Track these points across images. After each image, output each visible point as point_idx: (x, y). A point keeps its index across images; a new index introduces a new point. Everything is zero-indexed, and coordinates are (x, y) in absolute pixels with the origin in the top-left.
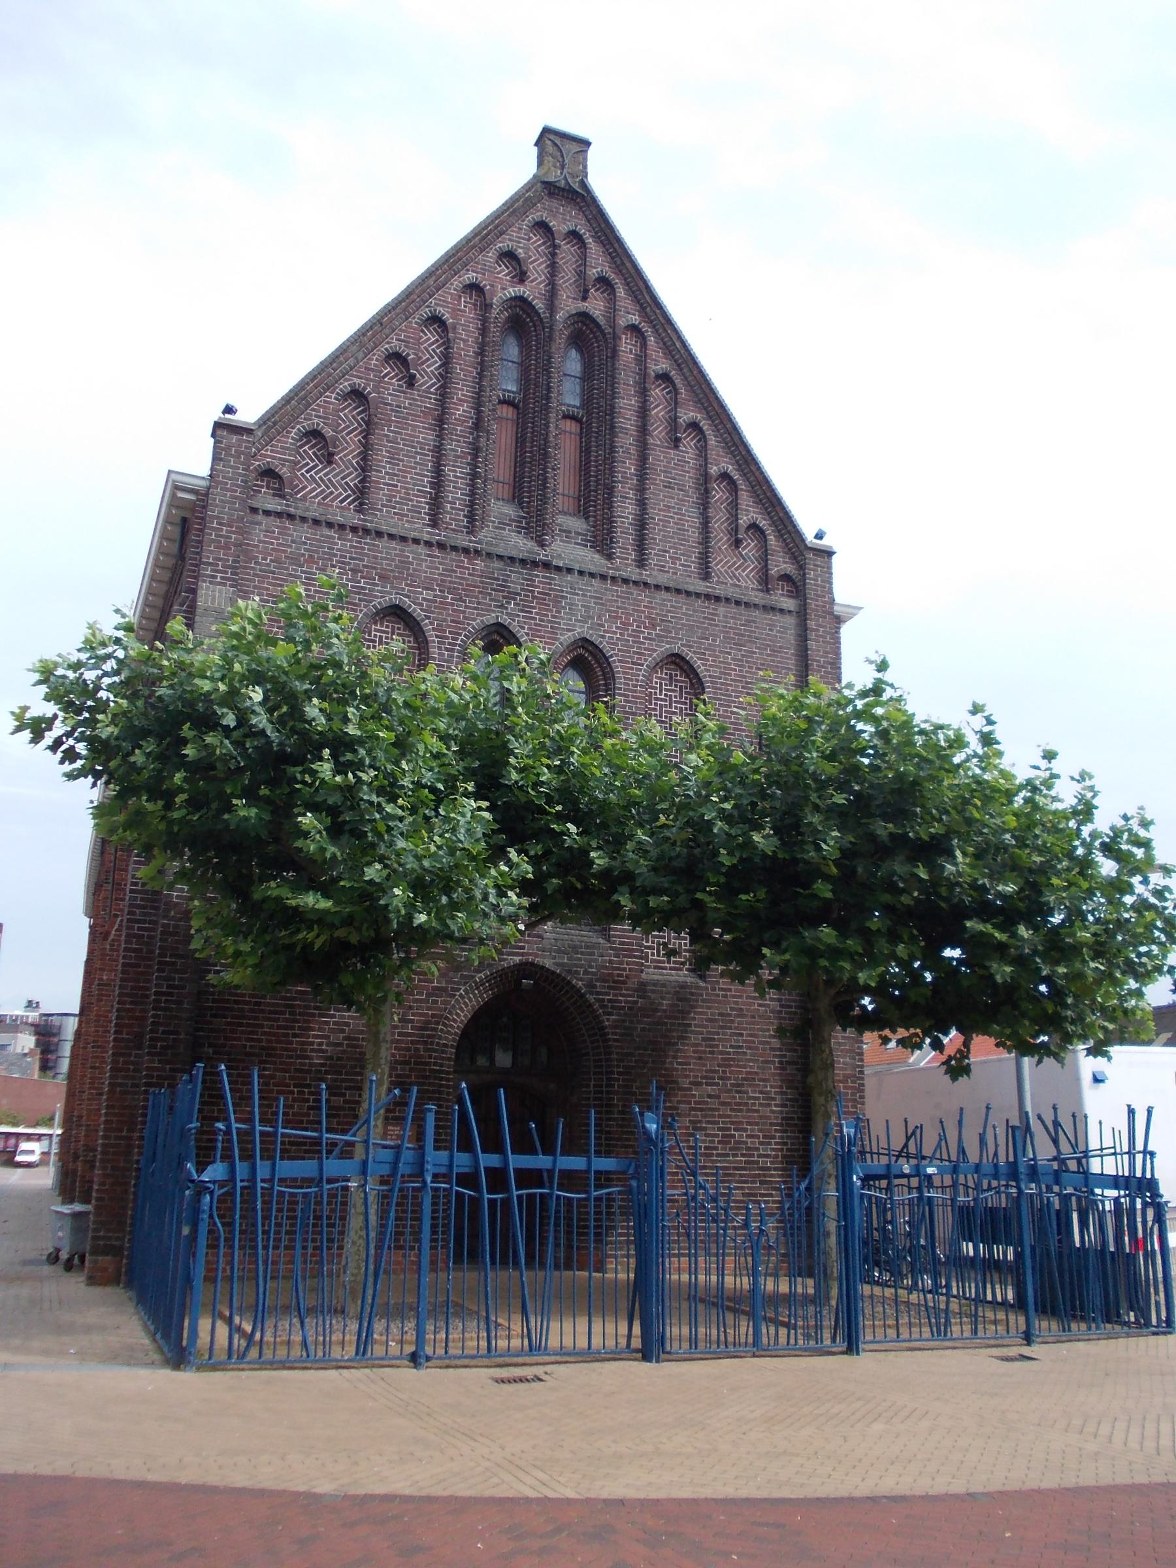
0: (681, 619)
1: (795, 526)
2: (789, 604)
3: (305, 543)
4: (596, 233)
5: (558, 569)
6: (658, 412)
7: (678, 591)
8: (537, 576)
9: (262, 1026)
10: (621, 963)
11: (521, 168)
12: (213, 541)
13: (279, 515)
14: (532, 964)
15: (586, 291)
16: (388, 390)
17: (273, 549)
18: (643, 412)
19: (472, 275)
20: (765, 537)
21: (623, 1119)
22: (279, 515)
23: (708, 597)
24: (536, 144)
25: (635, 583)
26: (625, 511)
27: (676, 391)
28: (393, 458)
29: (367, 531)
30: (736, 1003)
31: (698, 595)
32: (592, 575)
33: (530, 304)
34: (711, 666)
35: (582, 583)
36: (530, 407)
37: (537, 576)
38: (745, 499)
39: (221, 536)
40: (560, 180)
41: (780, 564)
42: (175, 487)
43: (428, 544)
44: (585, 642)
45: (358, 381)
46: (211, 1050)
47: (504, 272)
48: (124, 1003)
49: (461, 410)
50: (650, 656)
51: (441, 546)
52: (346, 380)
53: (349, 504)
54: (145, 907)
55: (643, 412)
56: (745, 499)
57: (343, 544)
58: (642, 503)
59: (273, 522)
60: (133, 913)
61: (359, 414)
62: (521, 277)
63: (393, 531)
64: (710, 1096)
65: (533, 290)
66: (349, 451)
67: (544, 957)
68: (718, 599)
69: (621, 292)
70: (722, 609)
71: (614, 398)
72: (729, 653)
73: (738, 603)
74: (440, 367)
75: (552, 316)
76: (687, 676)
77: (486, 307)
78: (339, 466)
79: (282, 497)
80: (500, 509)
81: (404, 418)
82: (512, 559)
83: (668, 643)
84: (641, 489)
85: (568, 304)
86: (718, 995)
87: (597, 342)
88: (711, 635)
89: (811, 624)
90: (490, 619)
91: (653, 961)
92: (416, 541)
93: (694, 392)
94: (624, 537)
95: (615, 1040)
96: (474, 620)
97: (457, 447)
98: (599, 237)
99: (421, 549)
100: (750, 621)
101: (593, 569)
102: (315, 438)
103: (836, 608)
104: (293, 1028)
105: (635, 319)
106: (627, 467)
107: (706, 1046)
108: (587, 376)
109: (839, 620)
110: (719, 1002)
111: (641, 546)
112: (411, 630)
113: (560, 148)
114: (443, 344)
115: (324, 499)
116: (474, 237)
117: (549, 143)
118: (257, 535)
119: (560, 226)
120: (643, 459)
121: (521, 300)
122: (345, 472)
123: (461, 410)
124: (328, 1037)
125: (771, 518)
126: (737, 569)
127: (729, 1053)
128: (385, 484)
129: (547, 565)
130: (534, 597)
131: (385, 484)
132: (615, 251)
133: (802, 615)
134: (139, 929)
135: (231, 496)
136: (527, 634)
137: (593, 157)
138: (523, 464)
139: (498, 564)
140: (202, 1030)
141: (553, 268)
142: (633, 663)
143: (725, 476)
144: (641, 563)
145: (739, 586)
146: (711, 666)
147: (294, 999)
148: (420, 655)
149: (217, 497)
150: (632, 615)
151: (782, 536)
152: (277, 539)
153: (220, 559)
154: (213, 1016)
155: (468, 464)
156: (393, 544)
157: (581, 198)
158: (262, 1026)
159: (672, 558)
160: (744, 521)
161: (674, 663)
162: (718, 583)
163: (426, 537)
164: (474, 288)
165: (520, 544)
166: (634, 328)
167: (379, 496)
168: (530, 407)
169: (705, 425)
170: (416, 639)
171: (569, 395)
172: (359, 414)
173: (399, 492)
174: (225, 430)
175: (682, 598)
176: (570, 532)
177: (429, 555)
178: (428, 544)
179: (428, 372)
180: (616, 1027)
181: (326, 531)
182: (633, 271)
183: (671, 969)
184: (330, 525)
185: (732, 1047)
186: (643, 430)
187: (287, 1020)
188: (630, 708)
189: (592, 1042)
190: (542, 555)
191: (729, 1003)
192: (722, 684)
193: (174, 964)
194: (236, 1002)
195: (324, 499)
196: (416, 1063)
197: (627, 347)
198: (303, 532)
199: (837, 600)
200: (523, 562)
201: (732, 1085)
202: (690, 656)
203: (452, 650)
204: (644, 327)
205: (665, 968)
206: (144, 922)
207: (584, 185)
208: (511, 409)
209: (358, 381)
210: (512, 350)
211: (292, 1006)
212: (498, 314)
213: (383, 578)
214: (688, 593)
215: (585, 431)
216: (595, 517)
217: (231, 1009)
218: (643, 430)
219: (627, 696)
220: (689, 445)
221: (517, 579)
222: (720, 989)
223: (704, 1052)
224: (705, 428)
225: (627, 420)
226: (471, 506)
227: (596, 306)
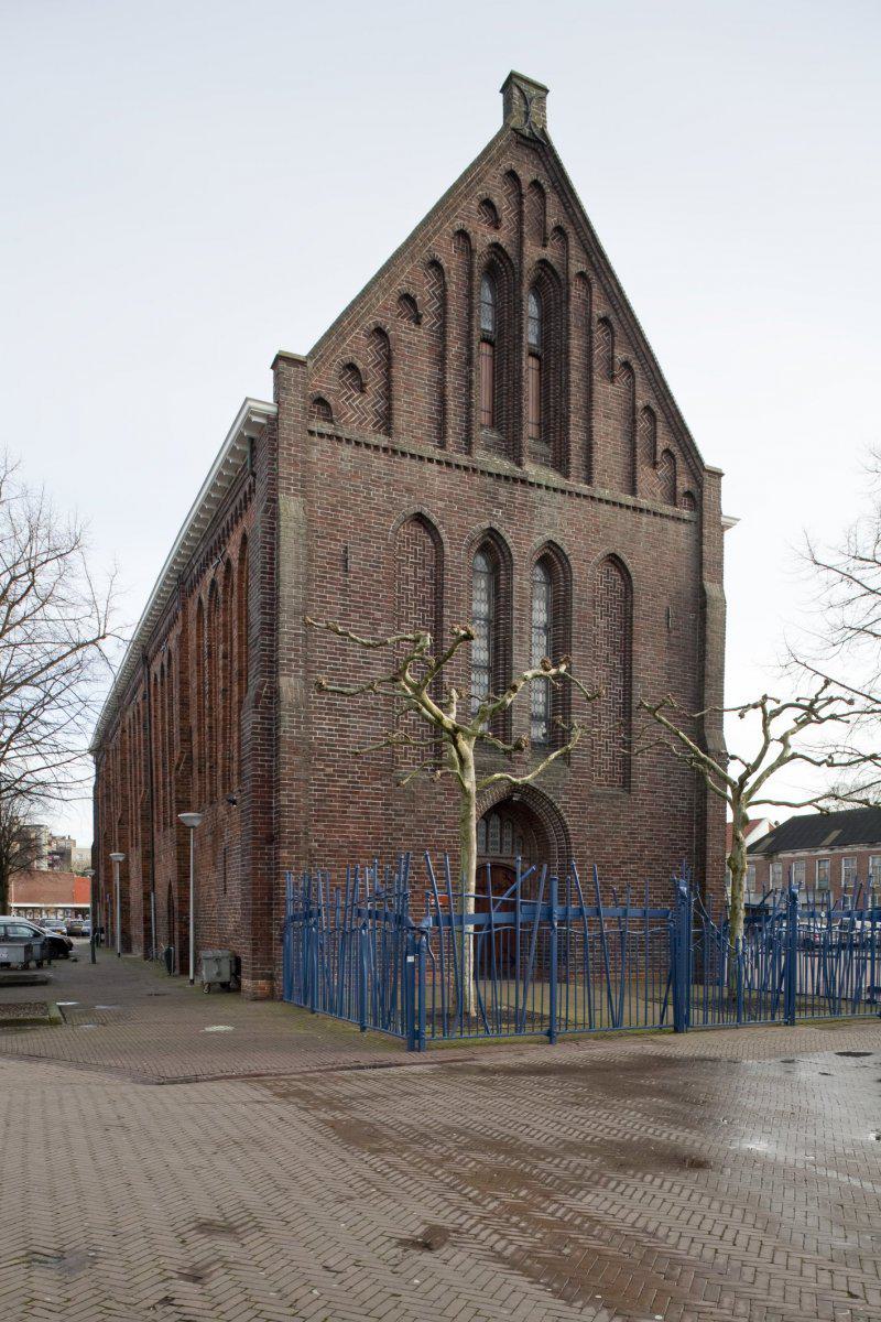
1: (697, 452)
2: (686, 514)
4: (553, 183)
5: (531, 484)
7: (614, 504)
9: (348, 827)
10: (577, 781)
11: (488, 121)
12: (285, 459)
13: (330, 437)
15: (545, 239)
16: (401, 330)
17: (329, 467)
18: (589, 352)
19: (459, 222)
20: (675, 460)
22: (330, 437)
23: (635, 508)
24: (502, 91)
25: (585, 496)
26: (576, 437)
27: (613, 333)
29: (395, 452)
31: (628, 507)
32: (555, 490)
36: (504, 342)
38: (661, 428)
39: (290, 455)
41: (684, 483)
43: (439, 462)
44: (551, 544)
48: (264, 629)
49: (454, 348)
54: (263, 734)
55: (589, 352)
58: (589, 431)
60: (265, 568)
62: (496, 224)
63: (413, 452)
64: (632, 871)
66: (374, 382)
68: (641, 510)
69: (572, 242)
70: (645, 519)
71: (569, 339)
73: (655, 514)
74: (438, 308)
75: (521, 262)
76: (620, 571)
77: (471, 252)
79: (331, 421)
80: (483, 435)
81: (414, 354)
82: (498, 476)
84: (588, 419)
85: (533, 252)
87: (553, 287)
89: (705, 531)
93: (627, 335)
94: (576, 461)
96: (474, 525)
97: (452, 380)
98: (555, 188)
99: (435, 467)
101: (555, 486)
102: (350, 370)
103: (723, 519)
106: (576, 399)
108: (544, 319)
109: (723, 528)
111: (589, 467)
112: (429, 532)
114: (440, 286)
115: (360, 423)
117: (516, 91)
118: (315, 454)
119: (526, 175)
120: (589, 392)
122: (369, 402)
123: (454, 348)
124: (391, 834)
125: (680, 445)
129: (523, 481)
133: (699, 525)
134: (261, 761)
135: (295, 421)
137: (551, 101)
139: (489, 480)
143: (647, 409)
144: (589, 481)
148: (436, 552)
149: (287, 422)
151: (686, 459)
153: (291, 474)
155: (464, 395)
156: (413, 462)
160: (660, 447)
161: (613, 562)
163: (437, 457)
165: (504, 466)
167: (400, 421)
168: (504, 342)
169: (635, 365)
171: (531, 335)
172: (381, 349)
174: (282, 361)
175: (617, 509)
177: (440, 472)
178: (439, 462)
179: (429, 310)
180: (574, 825)
182: (582, 221)
184: (368, 446)
186: (589, 368)
187: (365, 823)
190: (518, 472)
193: (291, 785)
194: (331, 811)
195: (360, 423)
197: (576, 291)
198: (347, 451)
200: (506, 478)
202: (624, 557)
203: (459, 549)
204: (591, 274)
207: (543, 133)
208: (488, 346)
209: (379, 319)
210: (486, 294)
211: (367, 813)
212: (479, 262)
213: (408, 490)
214: (621, 505)
215: (543, 369)
216: (554, 441)
217: (327, 816)
220: (622, 380)
221: (503, 492)
224: (634, 366)
226: (467, 431)
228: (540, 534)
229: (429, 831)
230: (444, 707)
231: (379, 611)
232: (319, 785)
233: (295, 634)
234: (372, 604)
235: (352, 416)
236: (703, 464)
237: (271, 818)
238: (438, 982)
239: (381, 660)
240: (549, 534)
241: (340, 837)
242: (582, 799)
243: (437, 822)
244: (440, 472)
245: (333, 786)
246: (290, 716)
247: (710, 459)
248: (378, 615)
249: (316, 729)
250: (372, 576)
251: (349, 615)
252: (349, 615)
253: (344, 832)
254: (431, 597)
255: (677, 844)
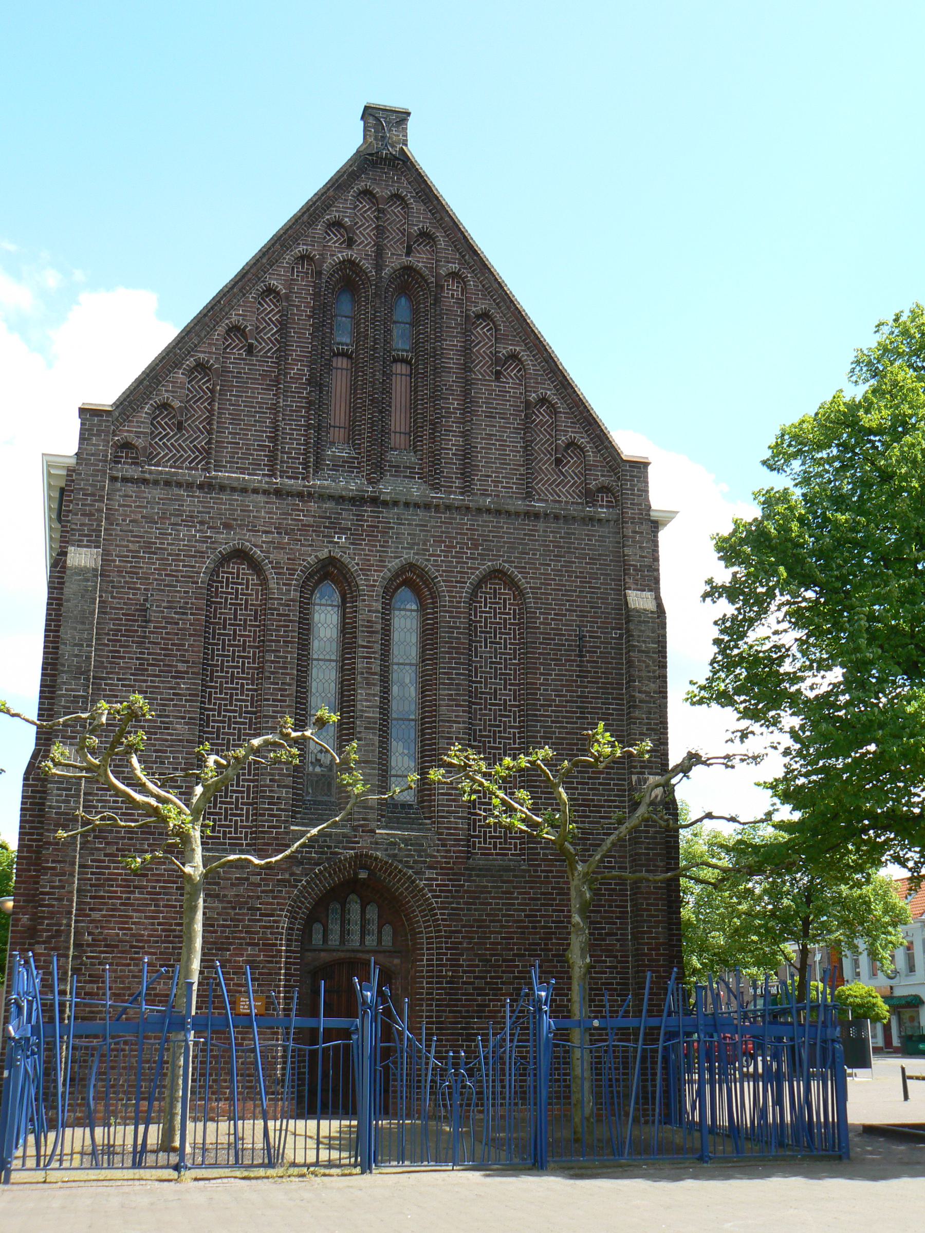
0: (503, 537)
3: (158, 503)
5: (385, 504)
6: (482, 349)
8: (366, 511)
9: (131, 917)
11: (349, 140)
14: (367, 855)
18: (466, 351)
19: (301, 248)
21: (451, 988)
24: (362, 118)
26: (452, 443)
28: (235, 420)
30: (558, 883)
31: (517, 514)
33: (358, 265)
34: (531, 578)
35: (408, 514)
37: (366, 511)
38: (564, 421)
40: (383, 167)
42: (50, 463)
43: (266, 492)
45: (202, 356)
46: (90, 938)
47: (334, 241)
50: (472, 574)
51: (278, 493)
52: (192, 356)
53: (197, 464)
54: (33, 822)
55: (466, 351)
56: (564, 421)
57: (191, 502)
59: (130, 489)
61: (204, 384)
65: (362, 254)
67: (377, 849)
69: (442, 243)
72: (549, 565)
78: (188, 432)
83: (490, 560)
85: (395, 260)
86: (540, 877)
88: (530, 549)
90: (324, 554)
91: (480, 848)
92: (255, 491)
95: (443, 920)
99: (261, 498)
100: (568, 534)
103: (652, 513)
104: (158, 918)
105: (455, 267)
107: (530, 922)
109: (656, 526)
110: (542, 883)
113: (384, 122)
116: (302, 215)
121: (350, 263)
126: (557, 486)
127: (551, 928)
128: (229, 443)
130: (363, 530)
131: (229, 443)
132: (435, 207)
133: (620, 522)
134: (29, 840)
136: (358, 564)
138: (355, 408)
140: (82, 921)
141: (380, 231)
142: (457, 582)
143: (543, 401)
145: (560, 502)
146: (531, 578)
147: (159, 894)
150: (456, 538)
152: (135, 502)
154: (91, 910)
157: (403, 164)
158: (131, 917)
159: (497, 479)
162: (539, 500)
164: (304, 258)
166: (454, 275)
170: (258, 576)
173: (241, 448)
174: (86, 413)
176: (399, 467)
177: (267, 503)
178: (266, 492)
179: (266, 345)
181: (176, 491)
183: (497, 854)
185: (553, 922)
186: (466, 368)
187: (154, 912)
188: (455, 622)
189: (424, 922)
191: (551, 883)
192: (542, 594)
194: (110, 898)
196: (264, 945)
197: (452, 290)
199: (654, 507)
201: (553, 955)
203: (290, 585)
205: (492, 854)
206: (32, 834)
209: (202, 356)
211: (157, 900)
214: (508, 513)
218: (466, 368)
219: (451, 612)
222: (542, 871)
223: (527, 927)
225: (452, 360)
227: (420, 260)
228: (396, 557)
229: (239, 921)
230: (216, 762)
231: (184, 662)
232: (97, 867)
233: (74, 696)
234: (176, 656)
235: (167, 454)
236: (619, 454)
237: (287, 946)
238: (284, 1127)
239: (184, 718)
240: (408, 556)
241: (120, 929)
242: (454, 874)
243: (249, 909)
244: (267, 503)
245: (115, 868)
246: (58, 789)
247: (628, 443)
248: (182, 667)
249: (98, 801)
250: (177, 624)
251: (147, 670)
252: (147, 670)
253: (126, 923)
254: (254, 641)
255: (604, 928)
